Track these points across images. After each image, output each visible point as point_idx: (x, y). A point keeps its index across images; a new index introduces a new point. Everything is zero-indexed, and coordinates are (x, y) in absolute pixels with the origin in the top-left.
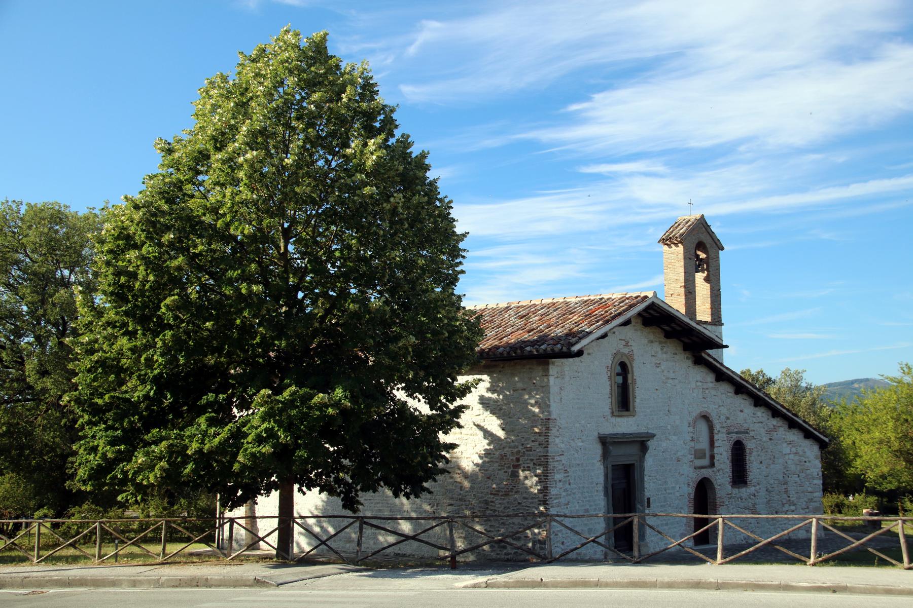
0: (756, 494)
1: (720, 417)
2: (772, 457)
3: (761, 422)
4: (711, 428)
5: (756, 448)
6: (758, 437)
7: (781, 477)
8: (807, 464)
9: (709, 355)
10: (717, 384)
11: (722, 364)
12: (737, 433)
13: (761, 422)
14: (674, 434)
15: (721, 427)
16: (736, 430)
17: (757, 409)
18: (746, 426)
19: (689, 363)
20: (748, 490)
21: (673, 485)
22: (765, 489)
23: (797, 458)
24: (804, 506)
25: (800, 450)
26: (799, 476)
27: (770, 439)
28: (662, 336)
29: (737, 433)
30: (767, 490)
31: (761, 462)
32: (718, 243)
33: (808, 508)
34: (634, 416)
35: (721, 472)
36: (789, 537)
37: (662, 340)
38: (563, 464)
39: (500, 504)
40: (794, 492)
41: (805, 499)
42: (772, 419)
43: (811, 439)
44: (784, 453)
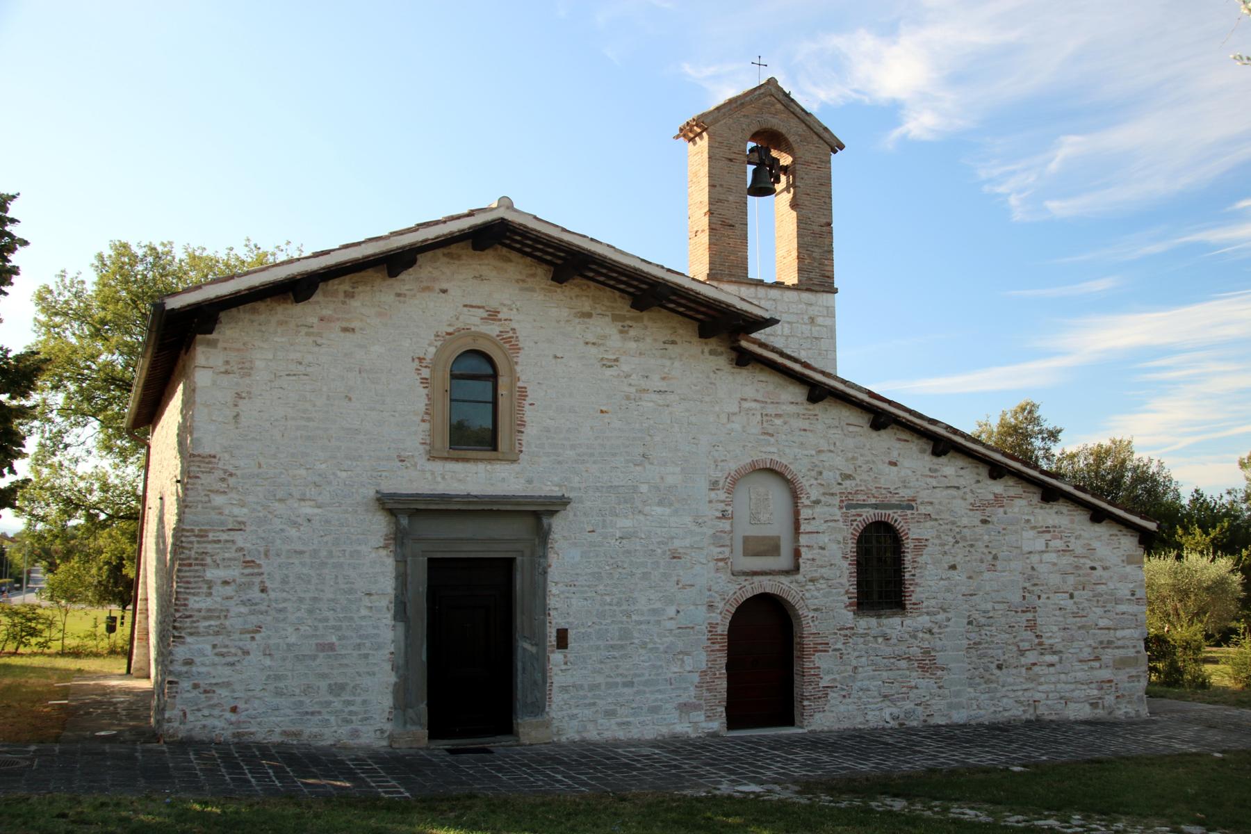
0: (935, 630)
1: (821, 473)
2: (990, 557)
3: (958, 488)
4: (794, 493)
5: (939, 537)
6: (946, 516)
7: (1016, 598)
8: (1099, 572)
9: (755, 342)
10: (811, 406)
11: (836, 378)
12: (876, 506)
13: (958, 488)
14: (660, 503)
15: (824, 494)
16: (873, 501)
17: (943, 460)
18: (906, 493)
19: (722, 362)
20: (907, 622)
21: (658, 605)
22: (966, 621)
23: (1065, 560)
24: (1085, 654)
25: (1077, 546)
26: (1072, 596)
27: (984, 522)
28: (624, 307)
29: (876, 506)
30: (970, 623)
31: (953, 567)
32: (826, 135)
33: (1097, 659)
34: (514, 461)
35: (822, 585)
36: (1037, 716)
37: (624, 312)
38: (241, 549)
39: (1212, 769)
40: (1055, 629)
41: (1091, 642)
42: (990, 482)
43: (1061, 500)
44: (1026, 549)
